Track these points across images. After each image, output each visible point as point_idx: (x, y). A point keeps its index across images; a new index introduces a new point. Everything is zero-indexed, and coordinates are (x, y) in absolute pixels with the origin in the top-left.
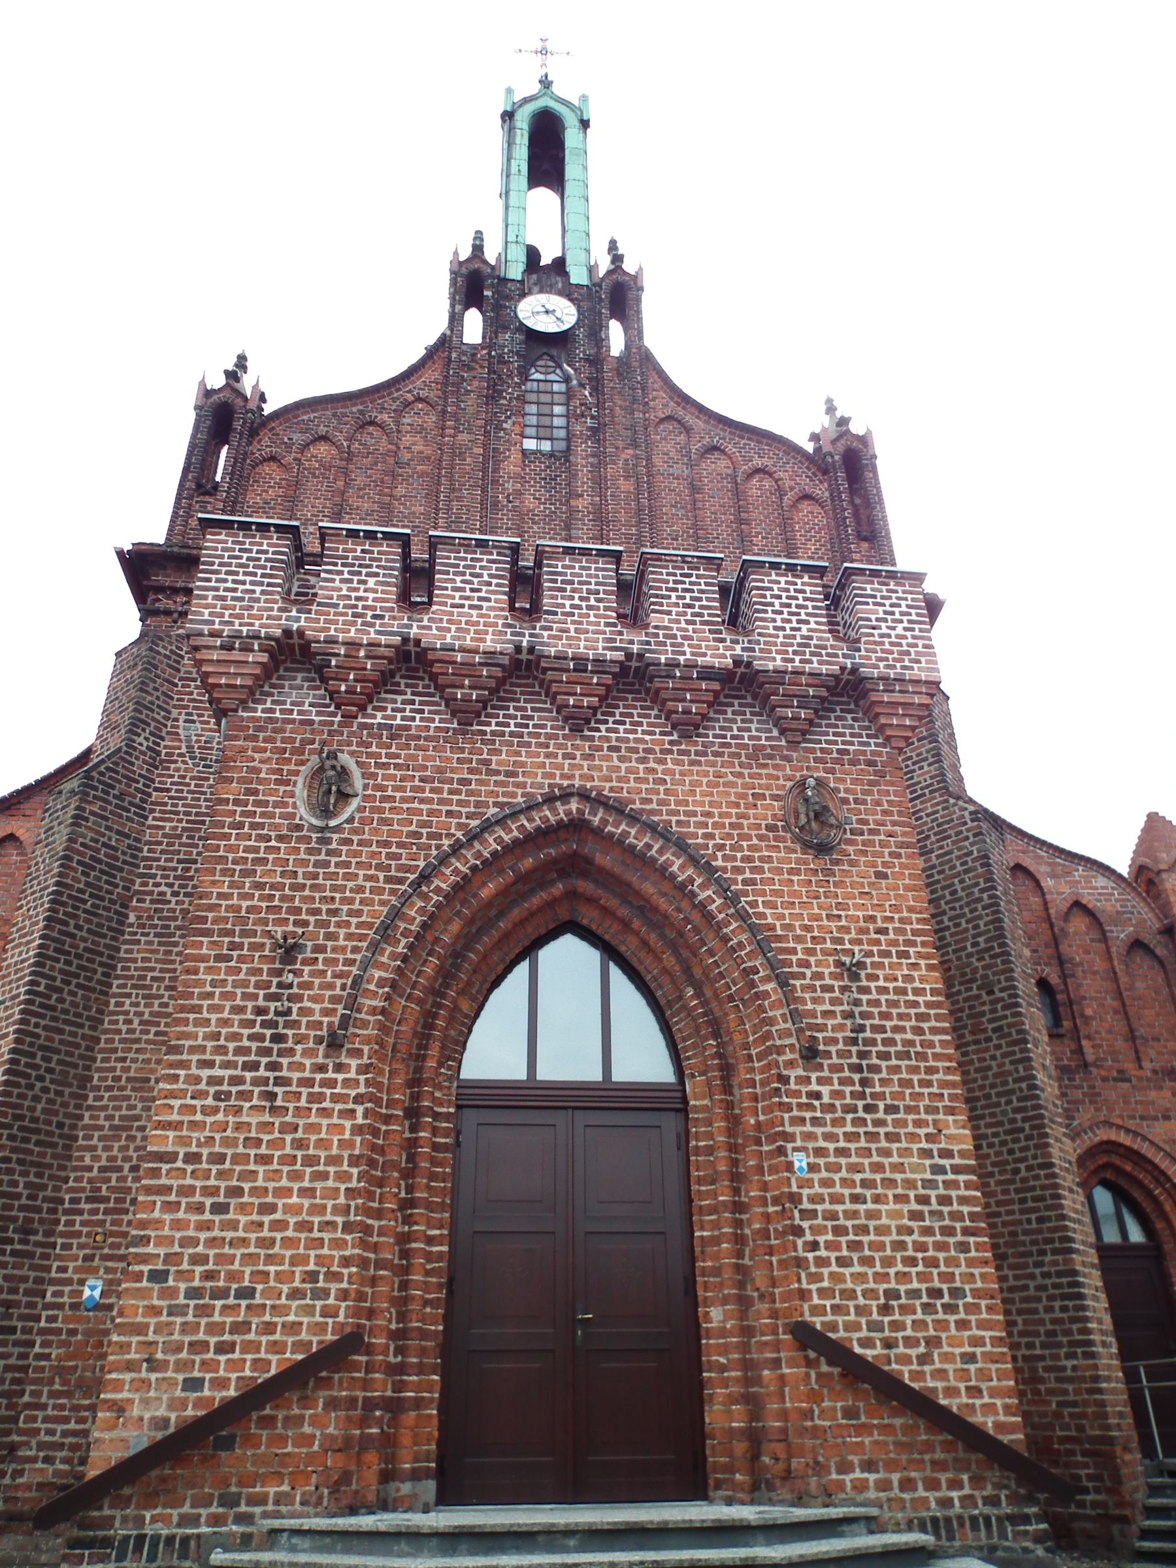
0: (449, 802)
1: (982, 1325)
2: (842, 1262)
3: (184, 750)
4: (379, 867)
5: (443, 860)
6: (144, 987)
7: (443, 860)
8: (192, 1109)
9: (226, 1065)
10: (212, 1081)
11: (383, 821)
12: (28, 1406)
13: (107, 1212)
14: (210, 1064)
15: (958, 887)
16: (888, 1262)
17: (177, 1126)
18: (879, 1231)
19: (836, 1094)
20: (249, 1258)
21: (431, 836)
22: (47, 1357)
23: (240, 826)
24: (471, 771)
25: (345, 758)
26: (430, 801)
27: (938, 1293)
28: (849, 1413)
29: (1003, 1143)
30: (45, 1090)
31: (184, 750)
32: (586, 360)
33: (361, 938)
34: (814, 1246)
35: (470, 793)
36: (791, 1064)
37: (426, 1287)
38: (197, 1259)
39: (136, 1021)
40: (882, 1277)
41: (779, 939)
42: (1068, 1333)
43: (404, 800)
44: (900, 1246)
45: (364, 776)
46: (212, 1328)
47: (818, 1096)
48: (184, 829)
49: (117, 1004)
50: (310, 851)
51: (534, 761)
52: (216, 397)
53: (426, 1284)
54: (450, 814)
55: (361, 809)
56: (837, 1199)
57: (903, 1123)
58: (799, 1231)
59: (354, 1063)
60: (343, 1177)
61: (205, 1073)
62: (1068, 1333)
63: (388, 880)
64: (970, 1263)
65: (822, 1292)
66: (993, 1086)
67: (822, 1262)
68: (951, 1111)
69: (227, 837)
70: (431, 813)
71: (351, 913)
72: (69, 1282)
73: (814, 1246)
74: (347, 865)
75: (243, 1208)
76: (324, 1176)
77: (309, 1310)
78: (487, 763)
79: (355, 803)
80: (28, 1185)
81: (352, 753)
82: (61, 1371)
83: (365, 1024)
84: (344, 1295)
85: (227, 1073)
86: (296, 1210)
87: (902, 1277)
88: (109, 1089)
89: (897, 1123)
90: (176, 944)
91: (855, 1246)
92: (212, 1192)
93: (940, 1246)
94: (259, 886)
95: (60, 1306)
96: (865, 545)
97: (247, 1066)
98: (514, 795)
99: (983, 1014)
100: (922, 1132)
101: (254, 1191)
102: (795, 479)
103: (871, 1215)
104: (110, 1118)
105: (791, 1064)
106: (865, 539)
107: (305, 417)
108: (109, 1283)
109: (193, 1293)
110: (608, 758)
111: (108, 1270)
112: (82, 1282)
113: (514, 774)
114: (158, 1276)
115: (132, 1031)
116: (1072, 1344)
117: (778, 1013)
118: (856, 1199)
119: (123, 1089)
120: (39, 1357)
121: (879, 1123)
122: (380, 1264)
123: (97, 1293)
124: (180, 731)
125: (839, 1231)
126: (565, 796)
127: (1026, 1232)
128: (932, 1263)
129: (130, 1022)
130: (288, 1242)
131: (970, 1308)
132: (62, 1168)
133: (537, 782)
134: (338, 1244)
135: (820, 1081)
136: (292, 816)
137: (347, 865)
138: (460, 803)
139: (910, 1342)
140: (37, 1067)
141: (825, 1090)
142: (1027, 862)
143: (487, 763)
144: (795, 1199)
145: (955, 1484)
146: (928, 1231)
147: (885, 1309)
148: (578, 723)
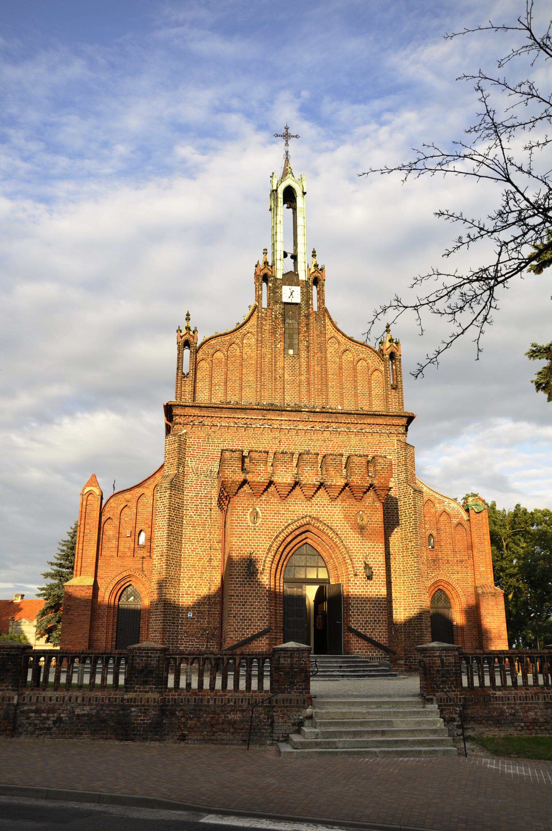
0: (280, 519)
1: (383, 626)
2: (358, 615)
3: (191, 471)
4: (267, 535)
5: (280, 533)
6: (190, 541)
7: (280, 533)
8: (236, 587)
9: (241, 578)
10: (239, 581)
11: (267, 524)
12: (180, 639)
13: (190, 597)
14: (238, 578)
15: (407, 513)
16: (367, 615)
17: (234, 590)
18: (366, 610)
19: (360, 583)
20: (250, 614)
21: (277, 527)
22: (182, 629)
23: (237, 526)
24: (285, 511)
25: (258, 509)
26: (276, 519)
27: (376, 621)
28: (357, 641)
29: (409, 582)
30: (173, 569)
31: (191, 471)
32: (305, 316)
33: (265, 551)
34: (353, 612)
35: (285, 517)
36: (351, 577)
37: (280, 619)
38: (241, 614)
39: (190, 550)
40: (365, 618)
41: (351, 550)
42: (417, 627)
43: (271, 519)
44: (369, 612)
45: (262, 513)
46: (245, 625)
47: (356, 584)
48: (195, 496)
49: (185, 546)
50: (252, 532)
51: (298, 508)
52: (184, 338)
53: (280, 618)
54: (281, 522)
55: (262, 521)
56: (358, 604)
57: (373, 589)
58: (351, 610)
59: (265, 578)
60: (265, 599)
61: (237, 580)
62: (417, 627)
63: (269, 538)
64: (383, 615)
65: (354, 621)
66: (409, 568)
67: (354, 615)
68: (383, 586)
69: (234, 529)
70: (277, 522)
71: (262, 546)
72: (184, 613)
73: (353, 612)
74: (260, 535)
75: (248, 605)
76: (262, 599)
77: (261, 623)
78: (288, 509)
79: (261, 520)
80: (174, 591)
81: (259, 507)
82: (185, 632)
83: (267, 570)
84: (267, 620)
85: (241, 580)
86: (257, 605)
87: (369, 618)
88: (186, 568)
89: (372, 589)
90: (197, 529)
91: (361, 612)
92: (242, 602)
93: (377, 612)
94: (242, 540)
95: (183, 618)
96: (394, 391)
97: (245, 578)
98: (294, 517)
99: (409, 549)
100: (377, 591)
101: (249, 602)
102: (374, 361)
103: (364, 607)
104: (187, 575)
105: (351, 577)
106: (394, 389)
107: (212, 342)
108: (193, 613)
109: (241, 620)
110: (315, 507)
111: (193, 610)
112: (187, 613)
113: (294, 512)
114: (234, 617)
115: (189, 553)
116: (418, 629)
117: (349, 567)
118: (362, 604)
119: (189, 568)
120: (180, 629)
121: (368, 589)
122: (272, 615)
123: (191, 615)
124: (189, 464)
125: (358, 610)
126: (306, 517)
127: (412, 604)
128: (375, 615)
129: (188, 550)
130: (256, 611)
131: (381, 623)
132: (179, 587)
133: (301, 513)
134: (265, 611)
135: (357, 581)
136: (247, 523)
137: (260, 535)
138: (283, 519)
139: (369, 629)
140: (171, 563)
141: (358, 583)
142: (432, 499)
143: (288, 509)
144: (350, 604)
145: (375, 652)
146: (375, 610)
147: (365, 624)
148: (309, 498)
